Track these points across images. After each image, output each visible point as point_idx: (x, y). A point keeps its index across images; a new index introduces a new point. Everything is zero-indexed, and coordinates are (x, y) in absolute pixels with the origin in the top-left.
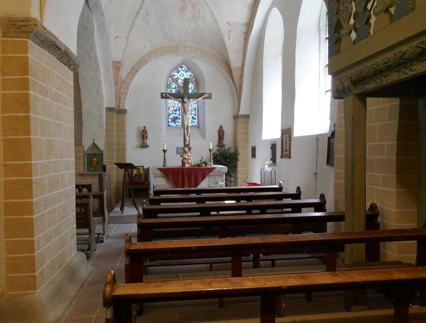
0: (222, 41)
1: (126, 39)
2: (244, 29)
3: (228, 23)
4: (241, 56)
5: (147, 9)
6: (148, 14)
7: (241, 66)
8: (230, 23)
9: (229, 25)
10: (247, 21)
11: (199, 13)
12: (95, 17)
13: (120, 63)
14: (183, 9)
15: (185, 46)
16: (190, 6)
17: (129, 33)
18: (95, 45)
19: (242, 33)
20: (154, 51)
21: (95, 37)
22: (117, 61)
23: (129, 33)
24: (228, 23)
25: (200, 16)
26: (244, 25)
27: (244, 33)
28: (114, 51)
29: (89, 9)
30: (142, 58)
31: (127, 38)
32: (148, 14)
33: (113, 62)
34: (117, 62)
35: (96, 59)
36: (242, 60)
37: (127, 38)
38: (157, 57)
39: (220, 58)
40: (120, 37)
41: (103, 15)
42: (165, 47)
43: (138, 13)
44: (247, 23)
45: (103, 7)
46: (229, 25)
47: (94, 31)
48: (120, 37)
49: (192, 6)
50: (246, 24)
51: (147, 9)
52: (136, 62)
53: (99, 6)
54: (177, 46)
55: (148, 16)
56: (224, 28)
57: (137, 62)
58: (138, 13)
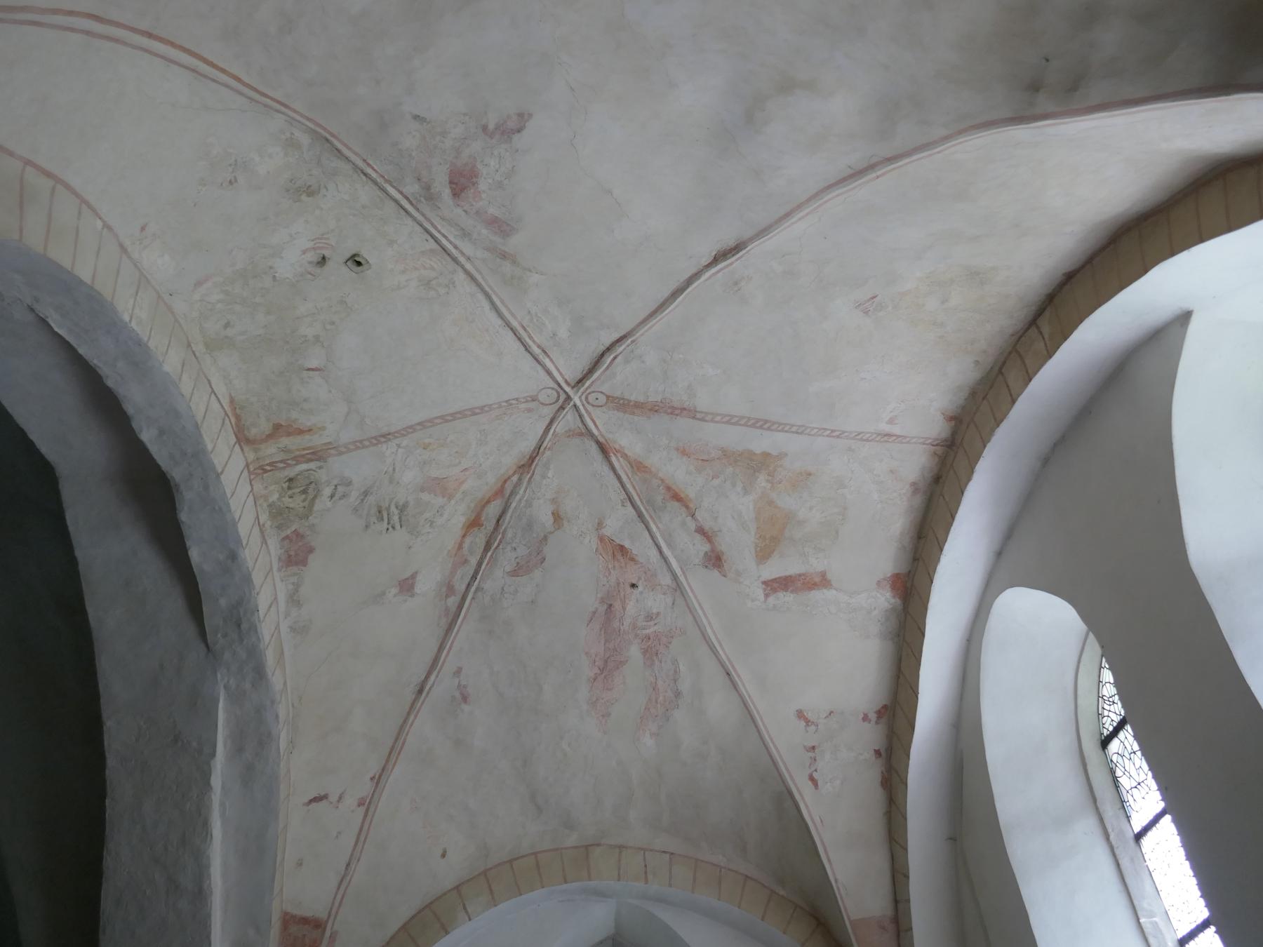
0: (784, 803)
1: (362, 810)
2: (872, 735)
3: (800, 714)
4: (879, 860)
5: (458, 672)
6: (465, 699)
7: (889, 912)
8: (809, 716)
9: (808, 722)
10: (881, 699)
11: (675, 681)
12: (225, 687)
13: (317, 925)
14: (608, 667)
15: (621, 847)
16: (635, 652)
17: (378, 780)
18: (206, 824)
19: (869, 755)
20: (485, 873)
21: (216, 781)
22: (308, 913)
23: (378, 780)
24: (800, 714)
25: (678, 694)
26: (873, 716)
27: (878, 753)
28: (300, 864)
29: (203, 646)
30: (429, 906)
31: (367, 804)
32: (465, 699)
33: (288, 920)
34: (305, 921)
35: (200, 895)
36: (886, 880)
37: (367, 804)
38: (494, 902)
39: (782, 893)
40: (333, 798)
41: (260, 673)
42: (535, 854)
43: (420, 692)
44: (885, 707)
45: (266, 631)
46: (808, 722)
47: (213, 754)
48: (333, 798)
49: (645, 652)
50: (880, 714)
51: (458, 672)
52: (394, 926)
53: (244, 626)
54: (587, 847)
55: (466, 708)
56: (786, 740)
57: (404, 927)
58: (420, 692)
